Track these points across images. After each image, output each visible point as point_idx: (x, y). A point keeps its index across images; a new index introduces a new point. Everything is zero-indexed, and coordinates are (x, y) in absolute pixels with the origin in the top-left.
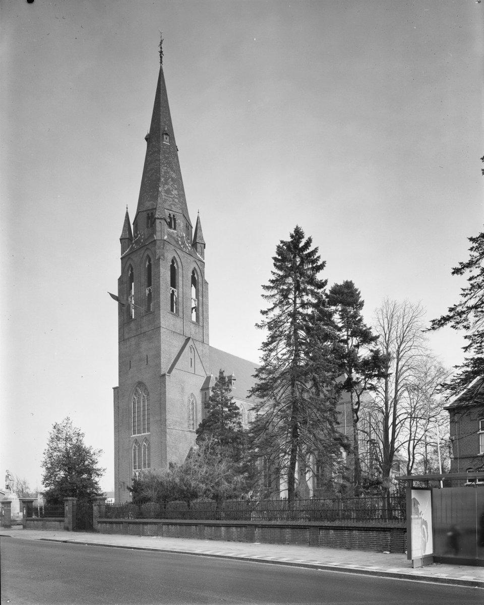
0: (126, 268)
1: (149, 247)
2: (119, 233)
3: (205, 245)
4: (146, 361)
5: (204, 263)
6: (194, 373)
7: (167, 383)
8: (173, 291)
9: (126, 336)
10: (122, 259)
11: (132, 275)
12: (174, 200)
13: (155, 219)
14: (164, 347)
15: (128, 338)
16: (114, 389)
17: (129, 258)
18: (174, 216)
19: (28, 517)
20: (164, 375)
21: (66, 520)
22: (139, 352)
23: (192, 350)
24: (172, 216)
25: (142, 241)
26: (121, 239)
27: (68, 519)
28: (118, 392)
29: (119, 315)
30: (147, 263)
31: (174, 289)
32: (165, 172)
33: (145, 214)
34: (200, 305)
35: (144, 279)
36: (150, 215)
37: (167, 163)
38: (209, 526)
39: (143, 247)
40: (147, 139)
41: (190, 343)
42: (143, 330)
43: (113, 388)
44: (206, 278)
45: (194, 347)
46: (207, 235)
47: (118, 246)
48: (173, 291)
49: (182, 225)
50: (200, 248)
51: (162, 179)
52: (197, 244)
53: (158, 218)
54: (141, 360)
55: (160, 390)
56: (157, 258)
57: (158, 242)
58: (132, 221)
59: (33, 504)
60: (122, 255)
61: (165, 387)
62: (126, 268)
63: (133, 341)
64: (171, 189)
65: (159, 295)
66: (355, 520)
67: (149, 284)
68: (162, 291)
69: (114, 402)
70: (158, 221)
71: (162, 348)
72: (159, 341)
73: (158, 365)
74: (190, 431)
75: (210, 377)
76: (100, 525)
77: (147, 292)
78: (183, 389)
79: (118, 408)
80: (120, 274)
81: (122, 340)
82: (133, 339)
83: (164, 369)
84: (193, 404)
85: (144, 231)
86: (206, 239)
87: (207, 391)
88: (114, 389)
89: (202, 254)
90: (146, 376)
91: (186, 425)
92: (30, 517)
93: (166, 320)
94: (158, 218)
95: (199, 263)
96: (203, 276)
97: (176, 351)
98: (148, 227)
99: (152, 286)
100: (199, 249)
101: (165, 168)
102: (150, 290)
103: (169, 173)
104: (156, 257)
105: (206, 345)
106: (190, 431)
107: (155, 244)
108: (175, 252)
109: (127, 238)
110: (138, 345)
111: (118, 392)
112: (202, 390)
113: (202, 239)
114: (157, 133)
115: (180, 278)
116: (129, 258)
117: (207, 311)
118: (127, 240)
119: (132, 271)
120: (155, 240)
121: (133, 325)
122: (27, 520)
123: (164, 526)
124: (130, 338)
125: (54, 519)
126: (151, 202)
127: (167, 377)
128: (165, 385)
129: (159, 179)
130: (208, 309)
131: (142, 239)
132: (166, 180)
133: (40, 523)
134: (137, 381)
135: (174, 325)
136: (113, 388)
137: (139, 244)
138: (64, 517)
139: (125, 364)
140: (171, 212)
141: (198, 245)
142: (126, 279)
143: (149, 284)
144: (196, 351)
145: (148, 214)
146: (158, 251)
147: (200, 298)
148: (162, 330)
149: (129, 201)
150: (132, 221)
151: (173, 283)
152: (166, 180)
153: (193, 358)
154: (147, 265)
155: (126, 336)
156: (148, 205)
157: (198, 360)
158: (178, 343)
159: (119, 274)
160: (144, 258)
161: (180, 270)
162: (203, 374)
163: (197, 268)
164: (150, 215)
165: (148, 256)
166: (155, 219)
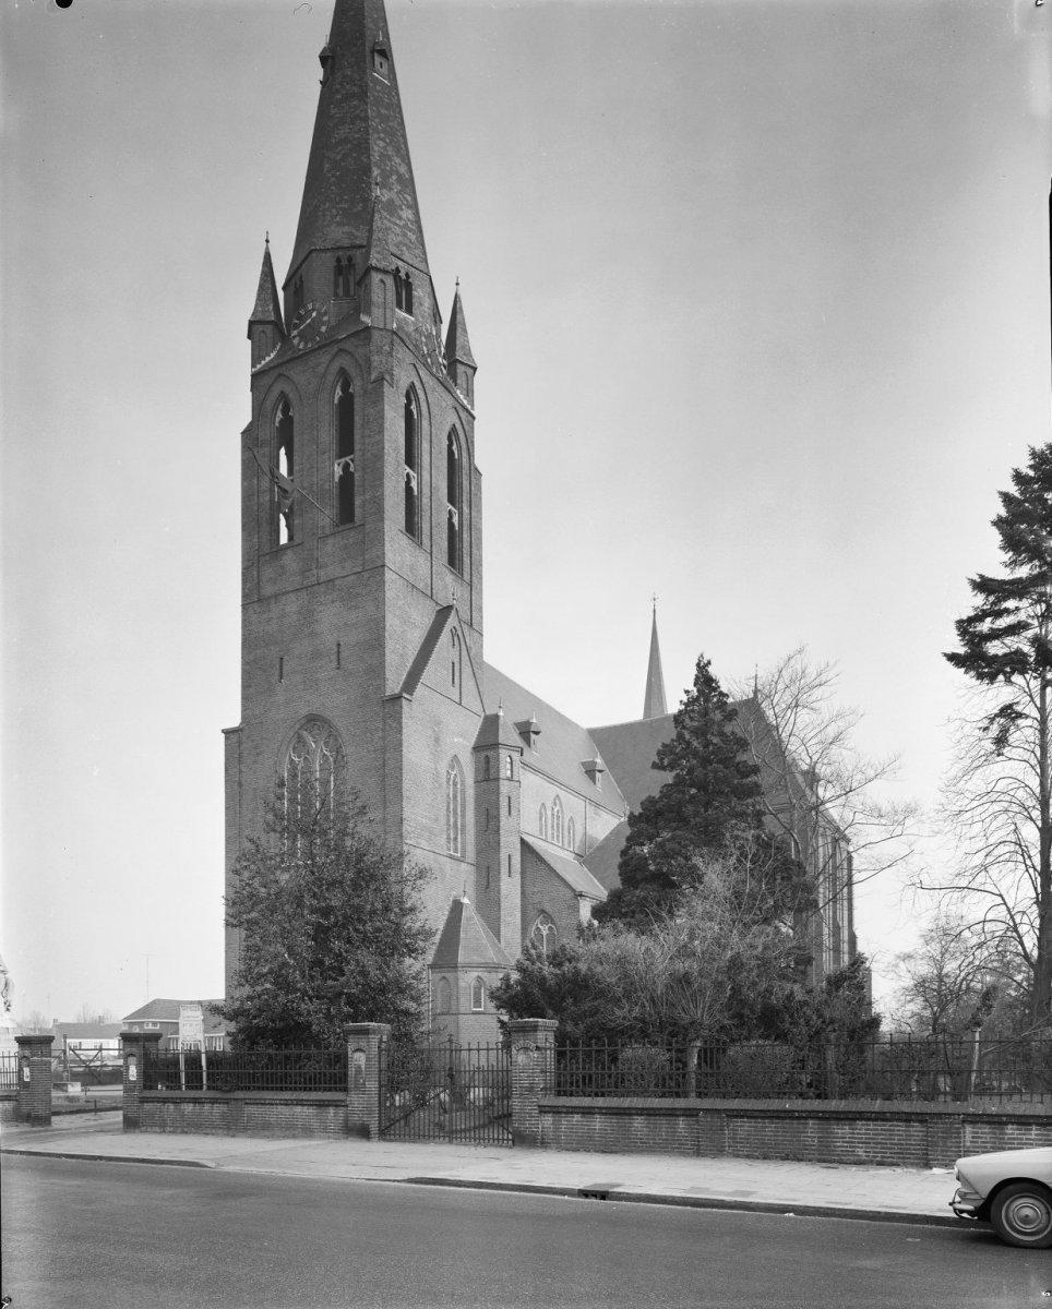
0: (269, 404)
1: (347, 346)
2: (245, 305)
3: (475, 369)
4: (334, 657)
5: (474, 418)
6: (457, 700)
7: (404, 720)
8: (408, 475)
9: (268, 590)
10: (254, 376)
11: (287, 422)
12: (405, 235)
13: (370, 269)
14: (392, 622)
15: (276, 596)
16: (227, 732)
17: (280, 375)
18: (407, 275)
19: (145, 1087)
20: (397, 698)
21: (356, 1100)
22: (313, 634)
23: (456, 638)
24: (402, 275)
25: (323, 329)
26: (251, 324)
27: (363, 1100)
28: (240, 743)
29: (243, 530)
30: (339, 392)
31: (411, 473)
32: (381, 155)
33: (328, 261)
34: (465, 528)
35: (328, 435)
36: (344, 263)
37: (384, 131)
38: (778, 1118)
39: (325, 346)
40: (325, 59)
41: (452, 621)
42: (323, 575)
43: (223, 731)
44: (478, 462)
45: (460, 633)
46: (480, 343)
47: (241, 351)
48: (408, 475)
49: (426, 305)
50: (464, 378)
51: (376, 172)
52: (455, 364)
53: (378, 270)
54: (316, 655)
55: (384, 738)
56: (373, 377)
57: (376, 335)
58: (280, 277)
59: (161, 1044)
60: (253, 366)
61: (400, 731)
62: (269, 404)
63: (292, 605)
64: (398, 203)
65: (381, 478)
66: (949, 1098)
67: (346, 445)
68: (389, 469)
69: (226, 770)
70: (376, 277)
71: (388, 625)
72: (380, 603)
73: (378, 671)
74: (451, 857)
75: (497, 716)
76: (548, 1120)
77: (338, 471)
78: (437, 740)
79: (240, 785)
80: (250, 419)
81: (254, 597)
82: (292, 597)
83: (394, 682)
84: (455, 784)
85: (323, 309)
86: (478, 357)
87: (491, 753)
88: (227, 732)
89: (469, 393)
90: (335, 701)
91: (443, 840)
92: (151, 1088)
93: (397, 551)
94: (378, 270)
95: (463, 415)
96: (470, 455)
97: (417, 638)
98: (336, 295)
99: (358, 453)
100: (461, 380)
101: (382, 144)
102: (346, 466)
103: (390, 160)
104: (370, 374)
105: (476, 634)
106: (451, 857)
107: (369, 339)
108: (414, 372)
109: (269, 322)
110: (308, 615)
111: (240, 743)
112: (477, 749)
113: (469, 354)
114: (355, 45)
115: (426, 445)
116: (280, 375)
117: (479, 548)
118: (270, 327)
119: (286, 411)
120: (367, 329)
121: (289, 560)
122: (143, 1100)
123: (969, 1129)
124: (284, 594)
125: (287, 1095)
126: (346, 229)
127: (404, 702)
128: (400, 723)
129: (367, 170)
130: (480, 539)
131: (323, 323)
132: (386, 175)
133: (218, 1109)
134: (304, 711)
135: (412, 568)
136: (223, 731)
137: (313, 340)
138: (345, 1090)
139: (263, 664)
140: (400, 263)
141: (460, 369)
142: (268, 432)
143: (346, 445)
144: (463, 643)
145: (338, 260)
146: (375, 358)
147: (465, 508)
148: (389, 575)
149: (270, 219)
150: (280, 277)
151: (411, 459)
152: (386, 175)
153: (456, 661)
154: (337, 398)
155: (268, 590)
156: (337, 233)
157: (467, 670)
158: (423, 619)
159: (245, 417)
160: (331, 378)
161: (425, 423)
162: (477, 707)
163: (458, 426)
164: (344, 263)
165: (283, 396)
166: (370, 269)
